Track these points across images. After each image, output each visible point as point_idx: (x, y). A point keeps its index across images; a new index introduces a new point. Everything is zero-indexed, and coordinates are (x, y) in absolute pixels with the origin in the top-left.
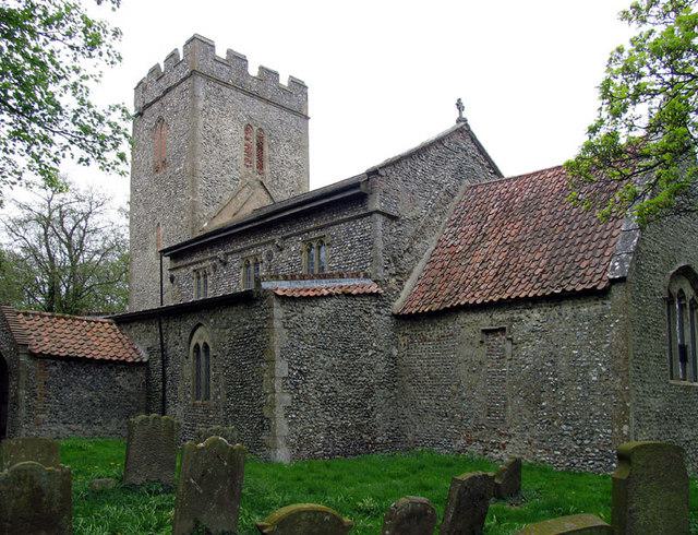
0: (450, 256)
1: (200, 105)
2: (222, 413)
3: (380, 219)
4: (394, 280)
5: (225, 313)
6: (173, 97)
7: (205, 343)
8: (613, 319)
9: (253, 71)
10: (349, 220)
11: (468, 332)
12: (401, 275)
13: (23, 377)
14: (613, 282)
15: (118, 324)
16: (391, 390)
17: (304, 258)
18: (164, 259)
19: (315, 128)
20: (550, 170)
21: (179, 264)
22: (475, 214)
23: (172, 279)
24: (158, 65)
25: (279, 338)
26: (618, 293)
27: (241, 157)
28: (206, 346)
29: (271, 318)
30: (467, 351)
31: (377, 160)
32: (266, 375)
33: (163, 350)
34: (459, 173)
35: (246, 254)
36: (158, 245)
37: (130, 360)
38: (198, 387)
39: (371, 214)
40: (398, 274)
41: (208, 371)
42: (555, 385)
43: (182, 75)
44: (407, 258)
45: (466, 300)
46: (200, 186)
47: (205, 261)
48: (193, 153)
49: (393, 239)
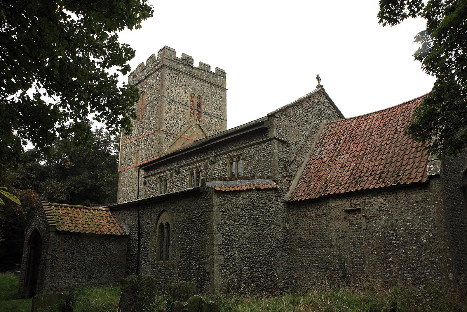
0: (319, 165)
1: (166, 83)
3: (276, 144)
4: (285, 180)
7: (167, 222)
8: (433, 202)
11: (335, 212)
12: (289, 177)
14: (431, 177)
15: (111, 211)
16: (285, 251)
18: (141, 171)
19: (229, 94)
20: (376, 113)
21: (149, 174)
22: (332, 139)
23: (145, 183)
24: (143, 63)
25: (217, 217)
26: (435, 186)
28: (167, 224)
29: (212, 205)
30: (336, 225)
31: (273, 109)
33: (139, 227)
34: (320, 116)
35: (192, 167)
37: (119, 234)
38: (161, 252)
39: (270, 140)
42: (397, 246)
44: (293, 167)
45: (367, 187)
47: (166, 172)
49: (284, 155)
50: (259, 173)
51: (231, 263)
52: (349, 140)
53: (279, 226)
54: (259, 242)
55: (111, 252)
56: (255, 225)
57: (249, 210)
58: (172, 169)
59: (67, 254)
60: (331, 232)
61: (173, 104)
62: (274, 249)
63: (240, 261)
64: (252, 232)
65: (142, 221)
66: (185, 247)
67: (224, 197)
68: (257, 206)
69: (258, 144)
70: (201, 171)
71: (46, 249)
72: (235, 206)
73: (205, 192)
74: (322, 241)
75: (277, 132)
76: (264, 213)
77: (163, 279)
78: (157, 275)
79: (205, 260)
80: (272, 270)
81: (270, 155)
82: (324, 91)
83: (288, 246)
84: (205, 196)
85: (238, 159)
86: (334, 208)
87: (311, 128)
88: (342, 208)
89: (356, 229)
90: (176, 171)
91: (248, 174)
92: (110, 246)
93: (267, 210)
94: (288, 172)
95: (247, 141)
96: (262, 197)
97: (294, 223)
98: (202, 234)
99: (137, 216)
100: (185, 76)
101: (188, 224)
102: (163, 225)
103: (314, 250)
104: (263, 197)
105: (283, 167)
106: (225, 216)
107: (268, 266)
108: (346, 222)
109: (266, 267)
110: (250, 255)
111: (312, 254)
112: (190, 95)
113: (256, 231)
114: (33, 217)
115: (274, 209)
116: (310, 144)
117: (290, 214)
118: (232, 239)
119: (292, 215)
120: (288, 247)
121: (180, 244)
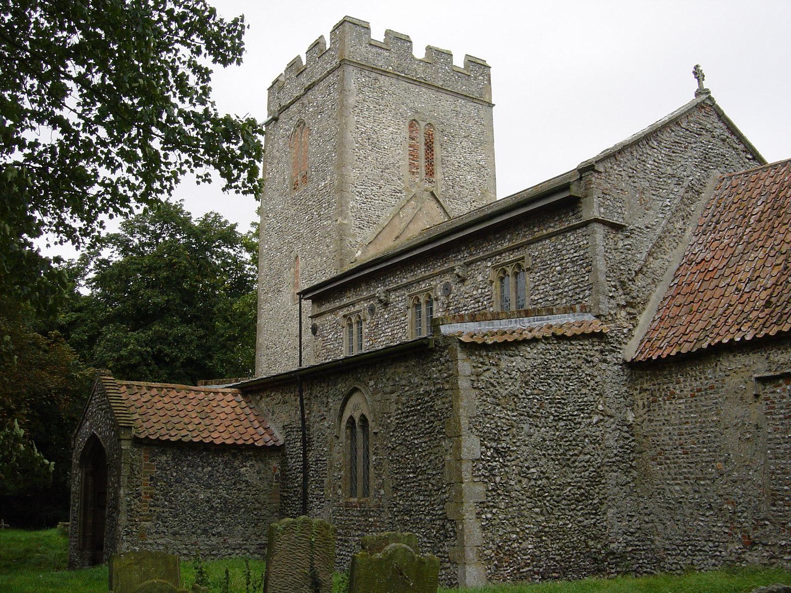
1: (352, 100)
2: (386, 516)
3: (600, 231)
4: (623, 313)
5: (390, 371)
6: (316, 95)
7: (363, 415)
9: (419, 53)
10: (555, 234)
11: (733, 381)
12: (633, 306)
13: (125, 471)
16: (626, 472)
17: (495, 288)
21: (324, 308)
22: (731, 215)
23: (314, 330)
24: (299, 57)
27: (405, 163)
28: (364, 419)
32: (448, 457)
35: (415, 290)
36: (296, 285)
37: (259, 444)
38: (353, 479)
39: (586, 224)
40: (629, 304)
41: (367, 457)
43: (329, 67)
44: (640, 282)
45: (730, 337)
46: (351, 204)
48: (341, 165)
49: (618, 257)
50: (564, 301)
51: (503, 499)
52: (769, 215)
53: (611, 416)
54: (564, 454)
55: (247, 482)
56: (554, 416)
57: (541, 382)
58: (373, 297)
59: (157, 485)
60: (726, 428)
61: (370, 148)
62: (599, 467)
63: (523, 494)
64: (547, 432)
65: (309, 414)
66: (402, 468)
67: (481, 356)
68: (559, 374)
69: (560, 234)
70: (437, 299)
71: (115, 476)
72: (507, 376)
73: (440, 348)
74: (706, 448)
75: (600, 206)
76: (573, 389)
77: (358, 536)
78: (346, 528)
79: (445, 493)
80: (596, 514)
81: (586, 258)
82: (714, 104)
83: (632, 461)
84: (441, 356)
85: (516, 270)
86: (731, 373)
87: (683, 190)
88: (750, 373)
89: (780, 419)
90: (381, 301)
91: (541, 303)
92: (244, 469)
93: (581, 382)
94: (628, 294)
95: (536, 229)
96: (568, 354)
97: (646, 409)
98: (436, 438)
99: (298, 403)
100: (394, 81)
101: (407, 417)
102: (354, 421)
103: (691, 468)
104: (572, 354)
105: (618, 284)
106: (484, 397)
107: (586, 506)
108: (758, 404)
109: (582, 509)
110: (544, 481)
111: (685, 478)
112: (407, 124)
113: (558, 430)
114: (86, 411)
115: (598, 379)
116: (680, 229)
117: (636, 389)
118: (503, 448)
119: (640, 393)
120: (634, 464)
121: (391, 461)
